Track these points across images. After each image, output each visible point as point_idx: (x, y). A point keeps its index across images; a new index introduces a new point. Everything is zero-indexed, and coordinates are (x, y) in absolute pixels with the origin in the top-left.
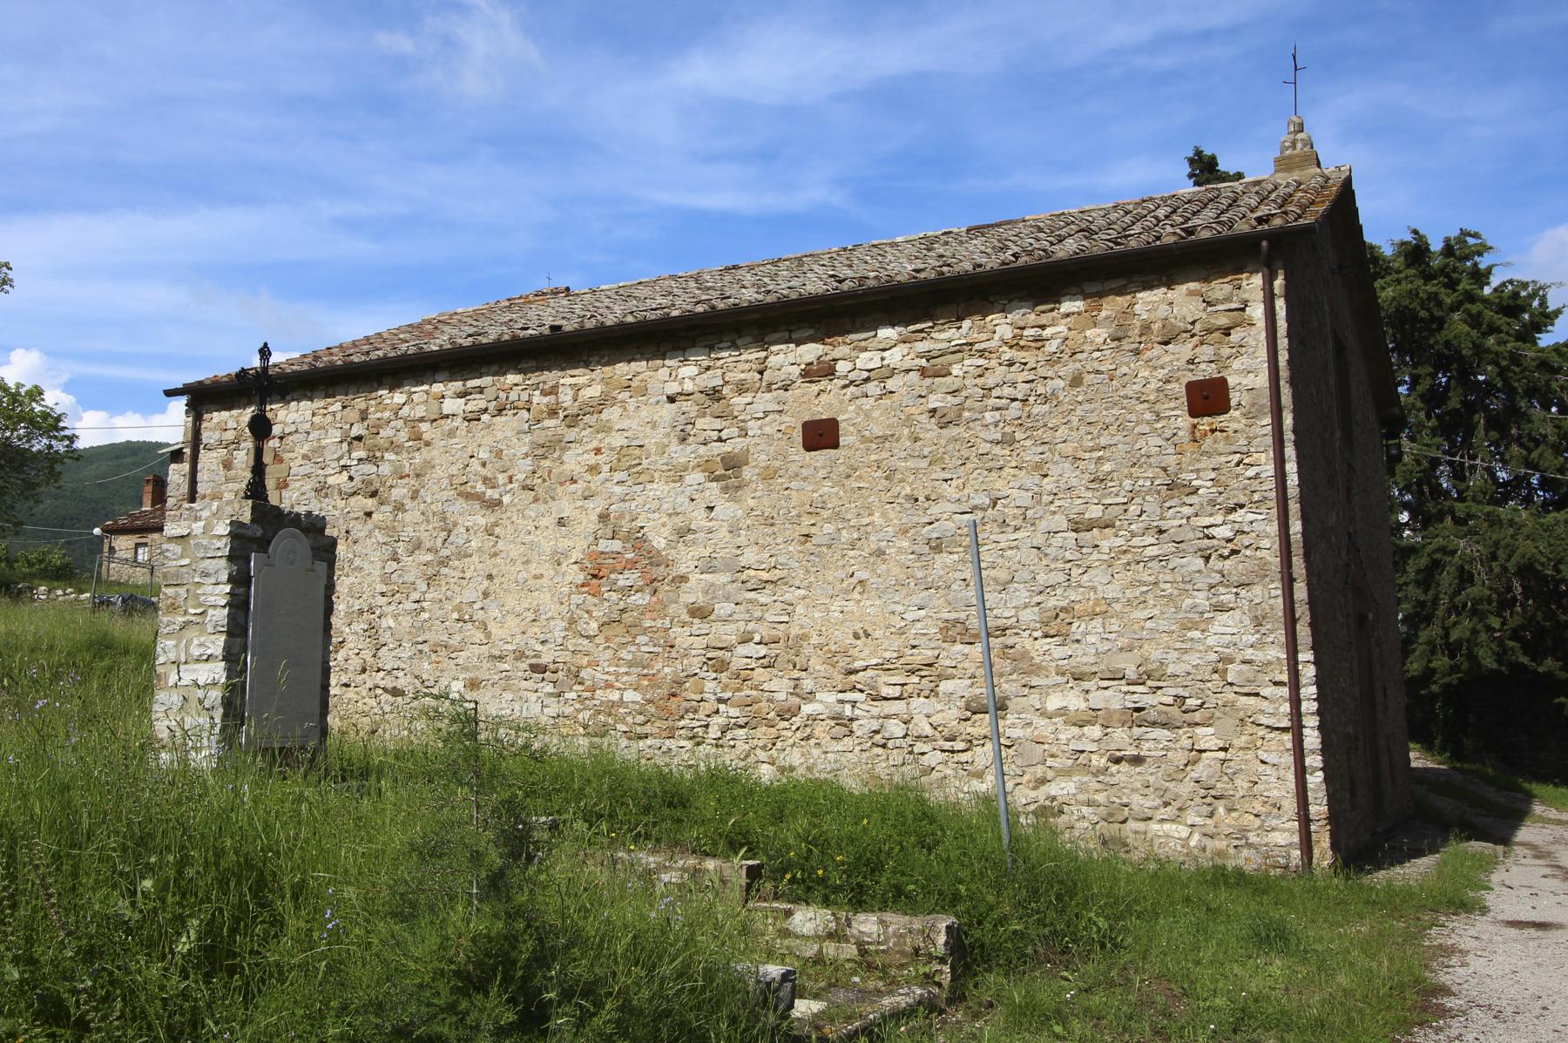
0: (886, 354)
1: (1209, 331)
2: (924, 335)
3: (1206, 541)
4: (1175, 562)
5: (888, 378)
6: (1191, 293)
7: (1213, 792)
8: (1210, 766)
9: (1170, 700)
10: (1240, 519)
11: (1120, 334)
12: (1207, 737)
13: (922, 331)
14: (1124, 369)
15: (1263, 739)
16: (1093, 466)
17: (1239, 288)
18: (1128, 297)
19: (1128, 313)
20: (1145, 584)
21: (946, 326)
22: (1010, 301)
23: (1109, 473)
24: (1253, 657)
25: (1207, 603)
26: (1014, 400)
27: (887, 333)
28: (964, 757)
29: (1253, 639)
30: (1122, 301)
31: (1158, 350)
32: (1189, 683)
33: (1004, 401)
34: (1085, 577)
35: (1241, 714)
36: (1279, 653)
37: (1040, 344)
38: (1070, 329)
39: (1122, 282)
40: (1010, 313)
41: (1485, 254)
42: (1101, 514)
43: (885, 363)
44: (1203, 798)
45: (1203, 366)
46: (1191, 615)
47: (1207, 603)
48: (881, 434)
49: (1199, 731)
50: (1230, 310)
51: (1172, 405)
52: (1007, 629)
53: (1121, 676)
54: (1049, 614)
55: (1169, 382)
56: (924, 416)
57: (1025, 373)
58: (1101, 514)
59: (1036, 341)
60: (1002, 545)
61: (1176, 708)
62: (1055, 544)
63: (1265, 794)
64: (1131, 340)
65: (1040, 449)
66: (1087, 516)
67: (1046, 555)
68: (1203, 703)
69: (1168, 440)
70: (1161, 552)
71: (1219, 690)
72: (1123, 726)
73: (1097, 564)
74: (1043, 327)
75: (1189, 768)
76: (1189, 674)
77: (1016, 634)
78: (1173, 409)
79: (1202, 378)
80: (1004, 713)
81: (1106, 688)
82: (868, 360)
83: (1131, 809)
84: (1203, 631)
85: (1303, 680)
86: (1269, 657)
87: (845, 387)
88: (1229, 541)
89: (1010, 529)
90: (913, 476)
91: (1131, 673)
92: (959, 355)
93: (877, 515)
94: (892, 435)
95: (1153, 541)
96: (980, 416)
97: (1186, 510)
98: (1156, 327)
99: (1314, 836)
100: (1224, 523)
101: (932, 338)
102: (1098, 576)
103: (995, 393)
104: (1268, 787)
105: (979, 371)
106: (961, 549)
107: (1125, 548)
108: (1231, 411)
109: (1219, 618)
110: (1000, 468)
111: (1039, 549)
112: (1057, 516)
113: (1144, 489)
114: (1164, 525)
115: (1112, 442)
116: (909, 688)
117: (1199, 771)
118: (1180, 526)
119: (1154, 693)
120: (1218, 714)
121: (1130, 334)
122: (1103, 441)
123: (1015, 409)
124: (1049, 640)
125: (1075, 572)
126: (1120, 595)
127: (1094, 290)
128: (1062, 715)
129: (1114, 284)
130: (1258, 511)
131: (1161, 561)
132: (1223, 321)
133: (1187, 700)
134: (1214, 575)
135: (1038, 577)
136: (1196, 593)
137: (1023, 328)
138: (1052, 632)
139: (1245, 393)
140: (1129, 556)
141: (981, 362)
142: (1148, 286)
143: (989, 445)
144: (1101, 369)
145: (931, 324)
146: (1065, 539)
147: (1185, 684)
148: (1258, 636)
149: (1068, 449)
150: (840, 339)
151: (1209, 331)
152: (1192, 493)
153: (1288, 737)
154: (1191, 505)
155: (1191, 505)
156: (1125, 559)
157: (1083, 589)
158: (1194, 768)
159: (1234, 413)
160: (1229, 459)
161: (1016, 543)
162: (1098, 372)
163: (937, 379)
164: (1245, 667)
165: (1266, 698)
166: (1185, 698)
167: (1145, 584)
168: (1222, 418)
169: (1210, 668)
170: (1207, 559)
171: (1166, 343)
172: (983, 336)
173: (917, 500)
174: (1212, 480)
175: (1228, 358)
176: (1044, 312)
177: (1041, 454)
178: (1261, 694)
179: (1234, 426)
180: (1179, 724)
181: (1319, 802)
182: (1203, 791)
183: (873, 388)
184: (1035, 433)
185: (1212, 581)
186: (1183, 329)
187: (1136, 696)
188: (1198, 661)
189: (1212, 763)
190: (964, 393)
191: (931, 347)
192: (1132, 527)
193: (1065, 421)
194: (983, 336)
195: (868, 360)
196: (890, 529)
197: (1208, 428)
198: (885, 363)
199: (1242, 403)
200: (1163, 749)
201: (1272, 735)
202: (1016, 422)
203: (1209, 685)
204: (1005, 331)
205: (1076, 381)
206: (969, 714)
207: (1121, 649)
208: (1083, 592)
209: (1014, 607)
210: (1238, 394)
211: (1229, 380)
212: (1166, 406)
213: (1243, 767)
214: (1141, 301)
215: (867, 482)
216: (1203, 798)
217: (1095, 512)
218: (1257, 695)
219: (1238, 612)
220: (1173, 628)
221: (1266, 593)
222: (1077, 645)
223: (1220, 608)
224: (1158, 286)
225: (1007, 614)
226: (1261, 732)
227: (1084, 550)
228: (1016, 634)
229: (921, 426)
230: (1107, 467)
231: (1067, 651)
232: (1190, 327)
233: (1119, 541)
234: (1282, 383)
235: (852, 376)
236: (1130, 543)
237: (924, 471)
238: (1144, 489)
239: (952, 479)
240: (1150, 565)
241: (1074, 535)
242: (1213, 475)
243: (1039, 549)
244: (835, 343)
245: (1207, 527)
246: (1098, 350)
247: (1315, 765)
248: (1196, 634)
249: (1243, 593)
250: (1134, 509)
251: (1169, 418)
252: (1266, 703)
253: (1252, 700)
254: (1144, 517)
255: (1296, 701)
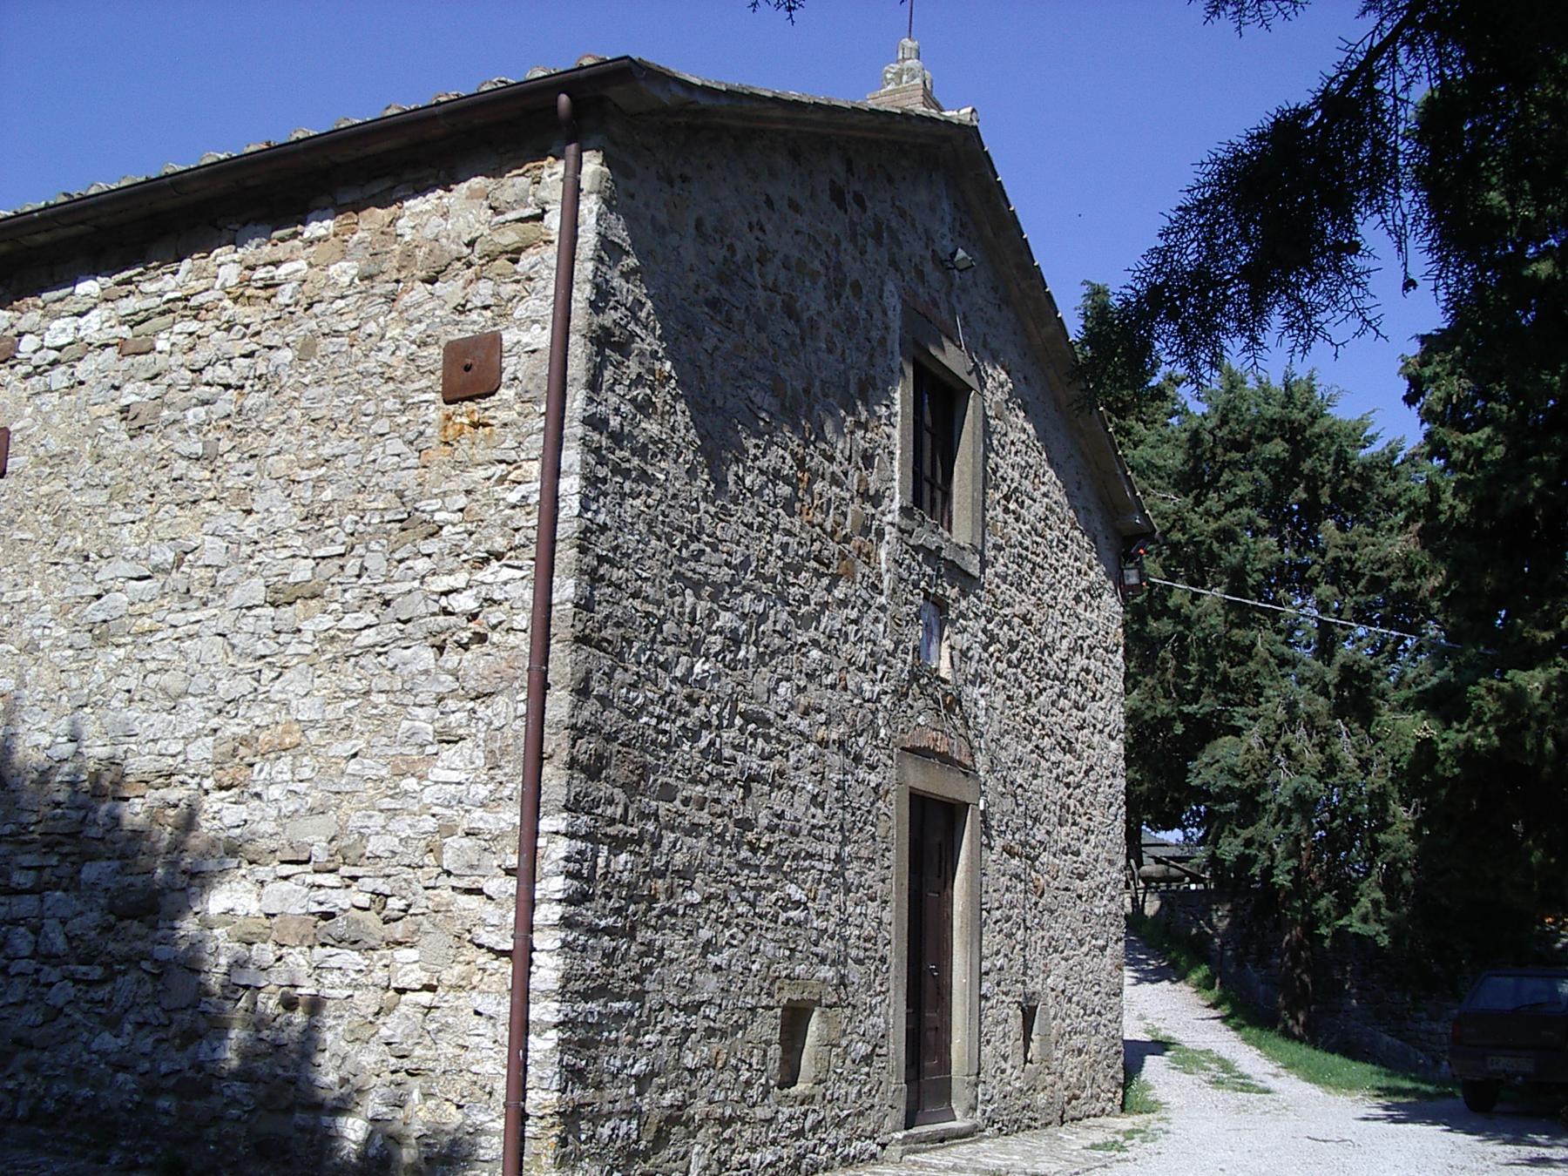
0: (82, 321)
1: (491, 257)
2: (132, 287)
3: (441, 618)
4: (397, 655)
5: (80, 359)
6: (472, 195)
7: (407, 1064)
8: (407, 1017)
9: (364, 900)
10: (490, 579)
11: (373, 270)
12: (409, 966)
13: (128, 281)
14: (371, 327)
15: (484, 970)
16: (309, 494)
17: (538, 183)
18: (394, 208)
19: (388, 231)
20: (349, 694)
21: (159, 272)
22: (245, 224)
23: (330, 503)
24: (481, 825)
25: (430, 728)
26: (227, 387)
27: (89, 287)
28: (102, 993)
29: (482, 792)
30: (380, 215)
31: (421, 291)
32: (393, 871)
33: (214, 389)
34: (278, 685)
35: (457, 929)
36: (511, 816)
37: (271, 291)
38: (310, 265)
39: (388, 183)
40: (242, 246)
41: (1415, 348)
42: (309, 575)
43: (82, 334)
44: (393, 1072)
45: (474, 316)
46: (406, 750)
47: (430, 728)
48: (57, 451)
49: (403, 954)
50: (521, 220)
51: (424, 383)
52: (172, 775)
53: (304, 857)
54: (223, 749)
55: (425, 344)
56: (113, 419)
57: (246, 340)
58: (309, 575)
59: (266, 287)
60: (180, 632)
61: (372, 913)
62: (245, 628)
63: (474, 1068)
64: (385, 277)
65: (247, 466)
66: (291, 580)
67: (234, 647)
68: (409, 906)
69: (411, 443)
70: (379, 638)
71: (431, 883)
72: (301, 944)
73: (295, 660)
74: (276, 264)
75: (382, 1019)
76: (394, 853)
77: (183, 783)
78: (424, 391)
79: (471, 334)
80: (155, 918)
81: (286, 878)
82: (60, 331)
83: (297, 1089)
84: (420, 778)
85: (544, 866)
86: (503, 824)
87: (27, 376)
88: (473, 617)
89: (192, 604)
90: (87, 519)
91: (320, 854)
92: (170, 317)
93: (36, 584)
94: (71, 452)
95: (371, 619)
96: (179, 416)
97: (422, 565)
98: (420, 254)
99: (526, 1167)
100: (469, 586)
101: (141, 292)
102: (295, 682)
103: (208, 375)
104: (478, 1056)
105: (188, 342)
106: (129, 639)
107: (332, 632)
108: (502, 390)
109: (444, 755)
110: (194, 502)
111: (224, 636)
112: (254, 580)
113: (370, 529)
114: (390, 590)
115: (338, 451)
116: (47, 875)
117: (390, 1027)
118: (410, 591)
119: (348, 887)
120: (427, 926)
121: (385, 267)
122: (326, 451)
123: (227, 402)
124: (224, 794)
125: (268, 674)
126: (319, 717)
127: (348, 199)
128: (227, 924)
129: (375, 188)
130: (516, 563)
131: (379, 654)
132: (510, 238)
133: (390, 901)
134: (443, 678)
135: (219, 685)
136: (418, 711)
137: (252, 268)
138: (226, 781)
139: (524, 356)
140: (338, 646)
141: (194, 326)
142: (420, 190)
143: (185, 463)
144: (342, 327)
145: (141, 269)
146: (258, 617)
147: (387, 871)
148: (491, 786)
149: (279, 465)
150: (29, 300)
151: (491, 257)
152: (432, 535)
153: (506, 966)
154: (429, 556)
155: (429, 556)
156: (332, 650)
157: (271, 706)
158: (388, 1020)
159: (506, 394)
160: (490, 473)
161: (197, 627)
162: (337, 333)
163: (138, 358)
164: (467, 842)
165: (489, 898)
166: (387, 896)
167: (349, 694)
168: (486, 403)
169: (423, 843)
170: (441, 649)
171: (432, 281)
172: (203, 284)
173: (87, 558)
174: (461, 510)
175: (510, 300)
176: (282, 240)
177: (248, 474)
178: (485, 890)
179: (503, 416)
180: (373, 943)
181: (545, 1084)
182: (393, 1060)
183: (59, 377)
184: (244, 440)
185: (441, 689)
186: (455, 255)
187: (322, 891)
188: (409, 832)
189: (410, 1012)
190: (167, 380)
191: (138, 306)
192: (348, 596)
193: (283, 417)
194: (203, 284)
195: (60, 331)
196: (48, 607)
197: (466, 420)
198: (82, 334)
199: (519, 375)
200: (349, 985)
201: (496, 964)
202: (223, 423)
203: (419, 872)
204: (230, 274)
205: (306, 351)
206: (112, 918)
207: (311, 809)
208: (273, 712)
209: (183, 738)
210: (514, 360)
211: (504, 337)
212: (416, 386)
213: (450, 1020)
214: (407, 213)
215: (33, 531)
216: (393, 1072)
217: (302, 571)
218: (479, 892)
219: (469, 743)
220: (384, 772)
221: (511, 709)
222: (257, 802)
223: (449, 739)
224: (432, 189)
225: (173, 749)
226: (483, 958)
227: (283, 638)
228: (183, 783)
229: (107, 435)
230: (327, 495)
231: (242, 812)
232: (466, 251)
233: (328, 621)
234: (573, 338)
235: (36, 360)
236: (340, 625)
237: (101, 509)
238: (370, 529)
239: (133, 522)
240: (362, 661)
241: (270, 611)
242: (462, 501)
243: (224, 636)
244: (24, 308)
245: (446, 594)
246: (343, 297)
247: (547, 1018)
248: (410, 784)
249: (481, 711)
250: (352, 565)
251: (417, 405)
252: (490, 907)
253: (474, 902)
254: (364, 579)
255: (527, 903)
